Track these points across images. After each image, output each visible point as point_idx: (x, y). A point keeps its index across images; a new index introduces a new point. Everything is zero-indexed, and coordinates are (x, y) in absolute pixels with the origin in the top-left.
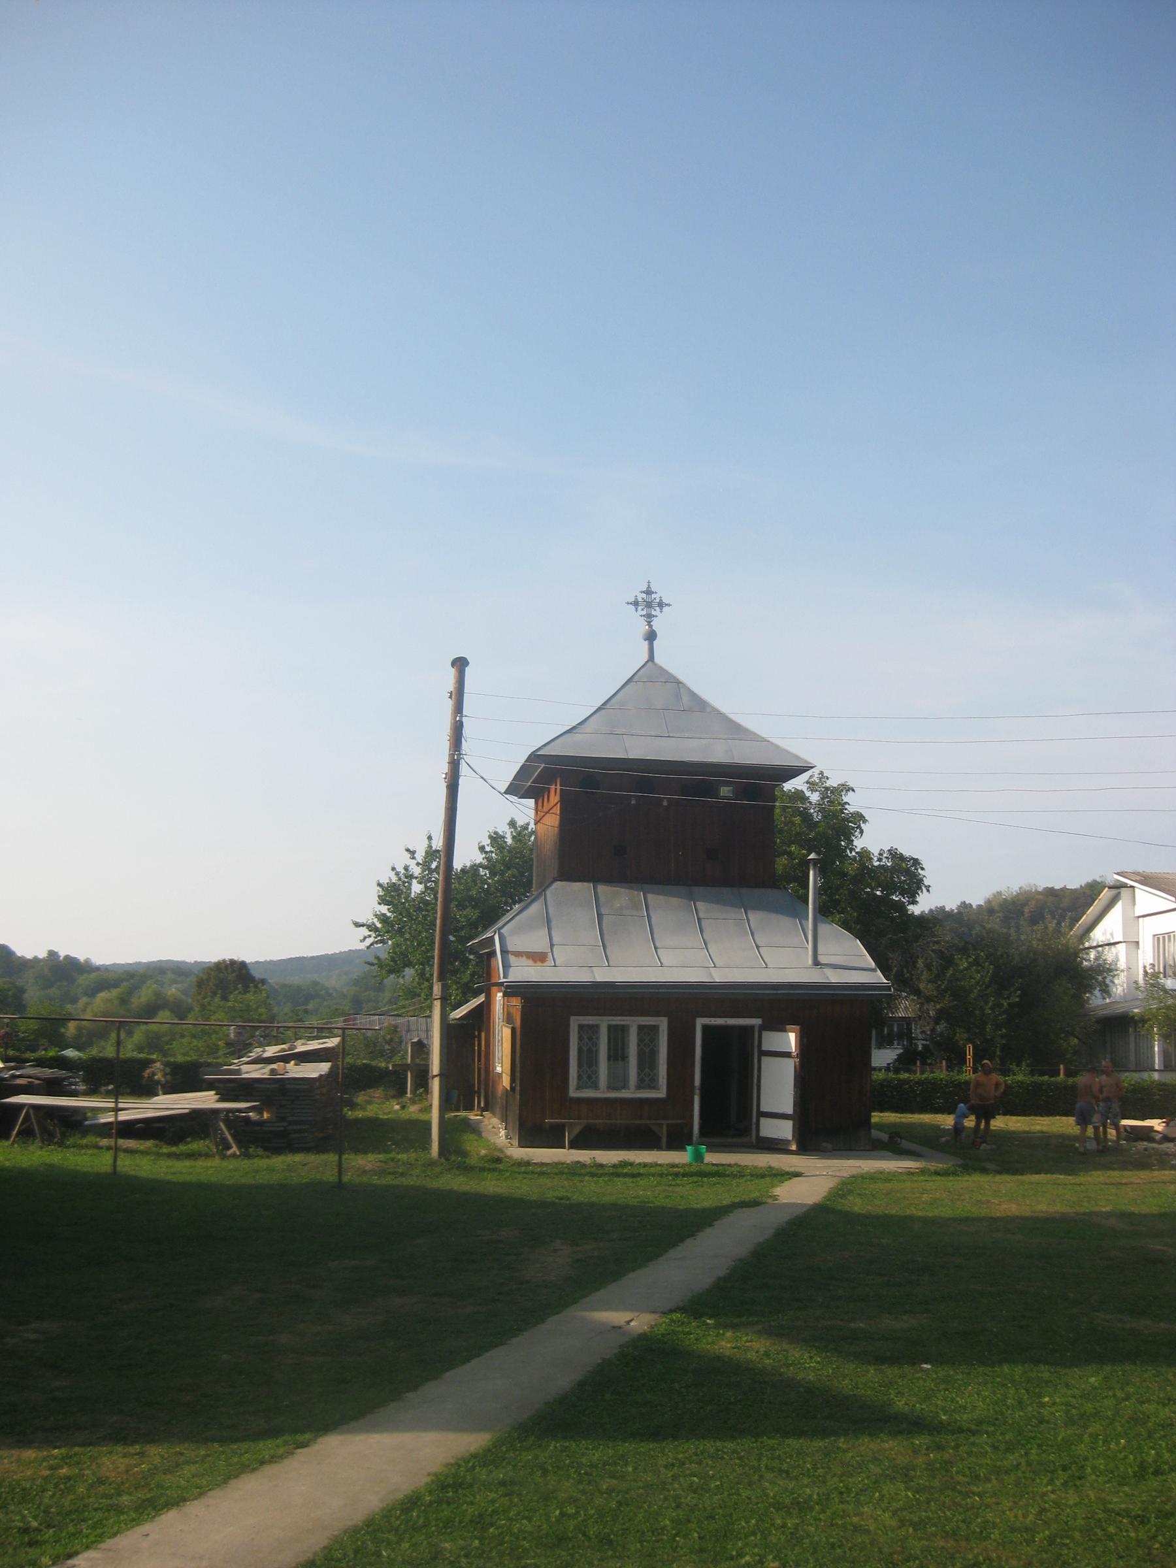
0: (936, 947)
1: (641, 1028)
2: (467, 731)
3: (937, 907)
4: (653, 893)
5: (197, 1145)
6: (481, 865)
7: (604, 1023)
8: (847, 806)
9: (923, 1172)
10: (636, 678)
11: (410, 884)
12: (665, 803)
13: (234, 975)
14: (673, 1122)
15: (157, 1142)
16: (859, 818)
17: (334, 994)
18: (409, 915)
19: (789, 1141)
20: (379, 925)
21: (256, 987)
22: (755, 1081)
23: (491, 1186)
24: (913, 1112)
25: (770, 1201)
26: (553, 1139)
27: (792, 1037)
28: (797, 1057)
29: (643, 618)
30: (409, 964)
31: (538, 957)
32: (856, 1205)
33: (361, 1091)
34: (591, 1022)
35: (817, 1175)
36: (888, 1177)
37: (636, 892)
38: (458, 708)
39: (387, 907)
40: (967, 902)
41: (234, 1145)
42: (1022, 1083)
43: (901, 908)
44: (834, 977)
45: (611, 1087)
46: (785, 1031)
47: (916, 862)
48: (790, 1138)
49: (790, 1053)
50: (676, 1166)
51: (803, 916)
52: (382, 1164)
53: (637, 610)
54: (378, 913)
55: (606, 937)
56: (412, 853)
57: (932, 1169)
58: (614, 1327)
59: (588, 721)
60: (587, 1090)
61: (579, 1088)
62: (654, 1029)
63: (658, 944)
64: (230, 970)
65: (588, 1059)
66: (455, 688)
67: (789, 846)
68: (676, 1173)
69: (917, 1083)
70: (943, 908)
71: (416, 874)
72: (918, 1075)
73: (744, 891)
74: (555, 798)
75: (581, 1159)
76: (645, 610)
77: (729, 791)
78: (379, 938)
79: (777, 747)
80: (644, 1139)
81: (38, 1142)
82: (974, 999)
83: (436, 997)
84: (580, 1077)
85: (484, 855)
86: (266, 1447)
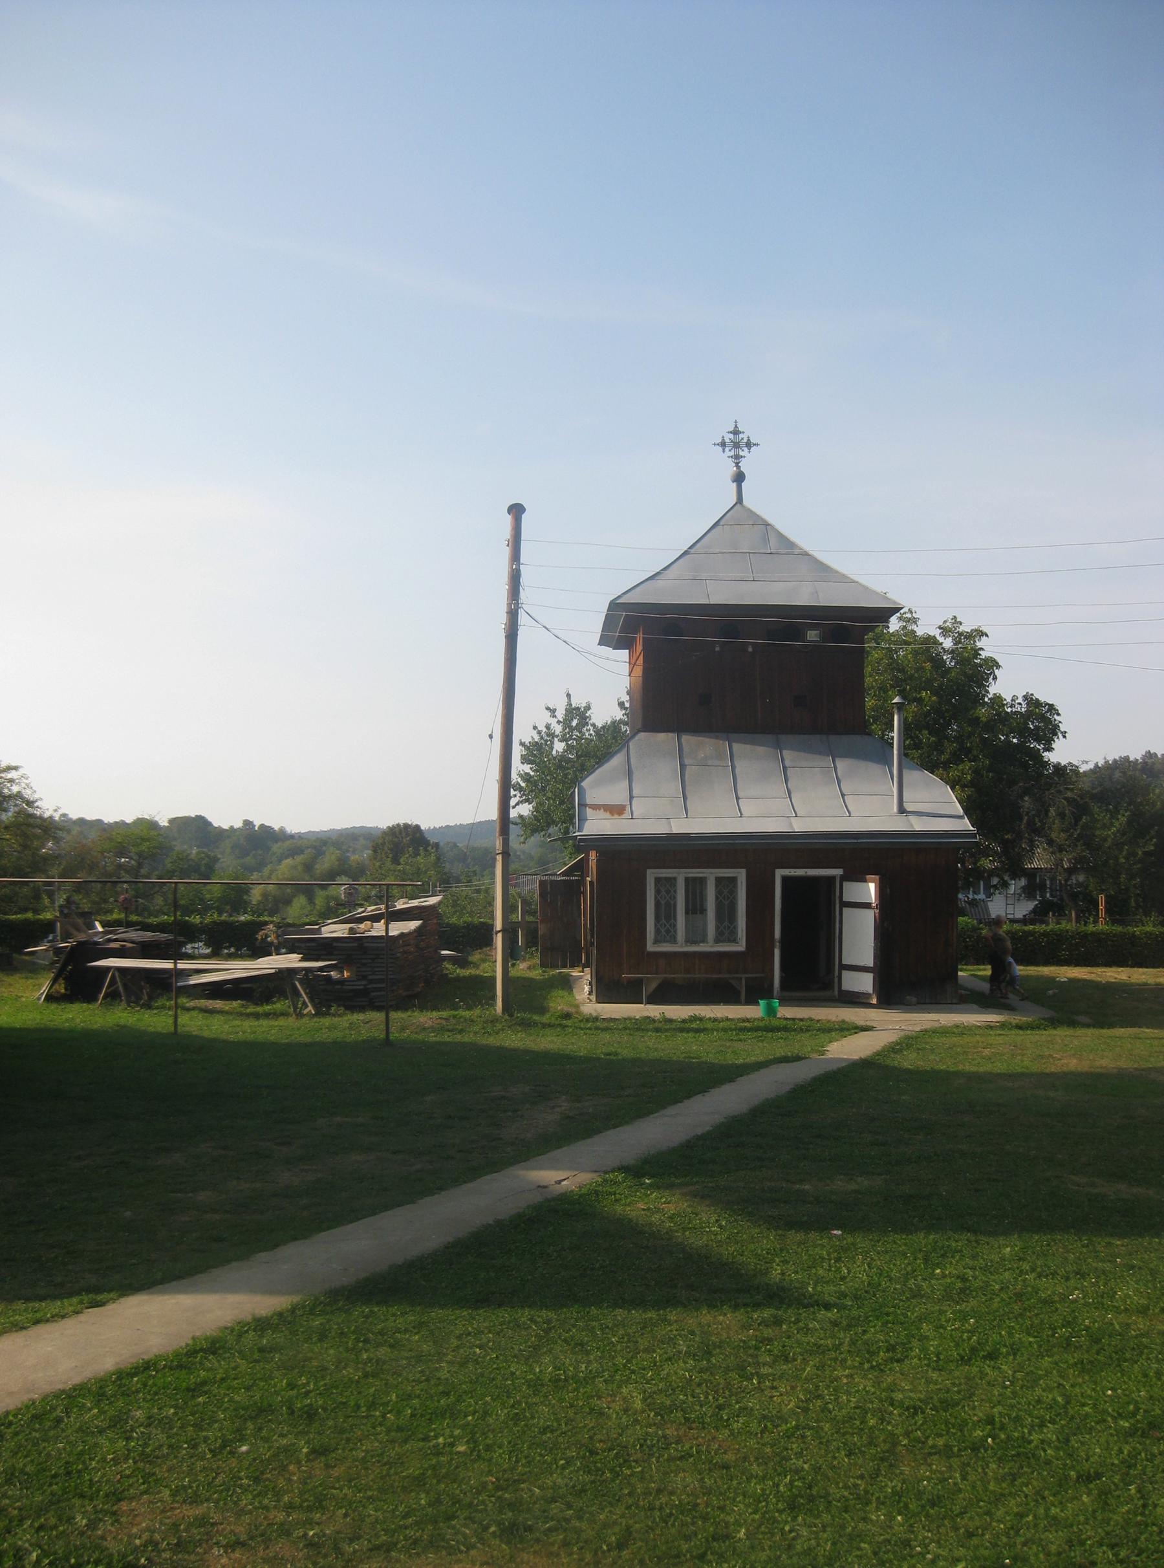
0: (1069, 794)
1: (719, 880)
2: (524, 580)
3: (1121, 757)
4: (738, 741)
5: (279, 1006)
6: (621, 721)
7: (681, 875)
8: (981, 652)
9: (1003, 1026)
10: (722, 523)
11: (552, 743)
12: (750, 649)
13: (408, 839)
14: (750, 975)
15: (244, 1002)
16: (993, 664)
17: (522, 857)
18: (550, 773)
19: (870, 994)
20: (523, 785)
21: (426, 850)
22: (837, 931)
23: (579, 1044)
24: (1037, 965)
25: (814, 1056)
26: (630, 993)
27: (872, 887)
28: (877, 908)
29: (730, 459)
30: (554, 822)
31: (616, 810)
32: (909, 1061)
33: (477, 949)
34: (668, 875)
35: (886, 1030)
36: (961, 1031)
37: (721, 742)
38: (516, 556)
39: (529, 766)
40: (1152, 752)
41: (309, 1004)
42: (1151, 934)
43: (1036, 756)
44: (918, 825)
45: (689, 941)
46: (865, 881)
47: (1051, 708)
48: (871, 992)
49: (870, 904)
50: (748, 1020)
51: (886, 760)
52: (444, 1022)
53: (724, 451)
54: (522, 772)
55: (688, 788)
56: (553, 712)
57: (1014, 1022)
58: (539, 1186)
59: (671, 568)
60: (665, 944)
61: (656, 941)
62: (733, 880)
63: (740, 794)
64: (404, 834)
65: (666, 913)
66: (511, 536)
67: (919, 693)
68: (743, 1028)
69: (1042, 934)
70: (1127, 758)
71: (557, 733)
72: (1051, 925)
73: (833, 738)
74: (639, 648)
75: (652, 1014)
76: (733, 451)
77: (816, 635)
78: (524, 797)
79: (866, 588)
80: (728, 996)
81: (124, 1004)
82: (1109, 848)
83: (498, 852)
84: (657, 931)
85: (624, 712)
86: (55, 1306)
